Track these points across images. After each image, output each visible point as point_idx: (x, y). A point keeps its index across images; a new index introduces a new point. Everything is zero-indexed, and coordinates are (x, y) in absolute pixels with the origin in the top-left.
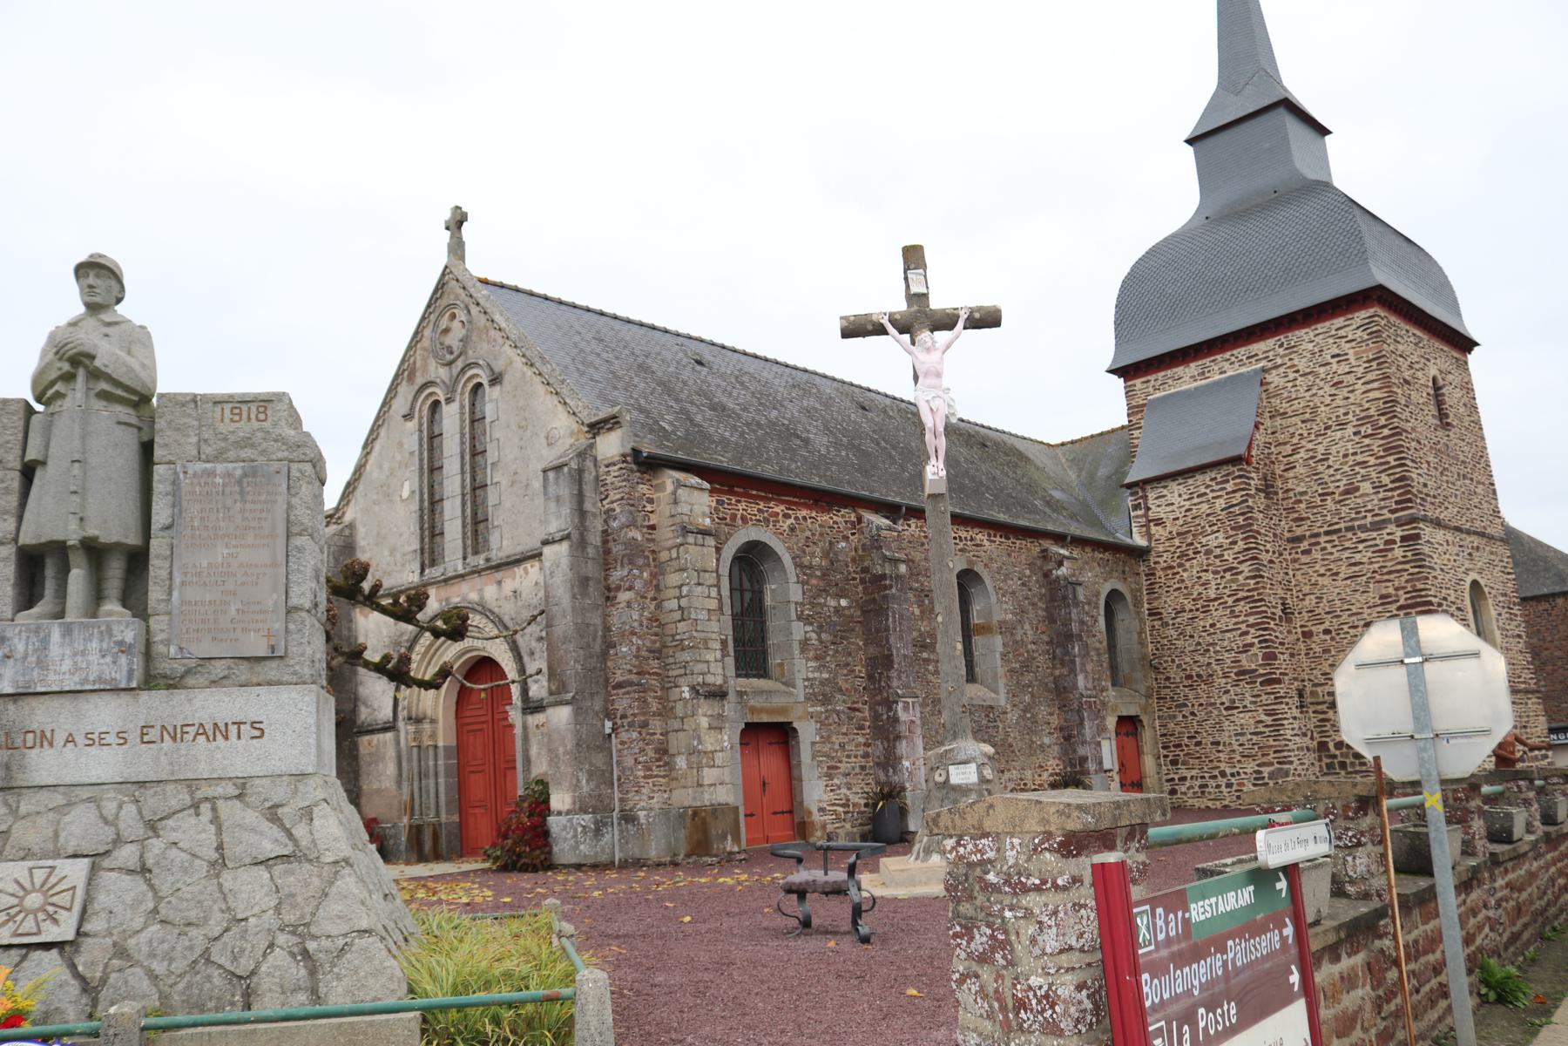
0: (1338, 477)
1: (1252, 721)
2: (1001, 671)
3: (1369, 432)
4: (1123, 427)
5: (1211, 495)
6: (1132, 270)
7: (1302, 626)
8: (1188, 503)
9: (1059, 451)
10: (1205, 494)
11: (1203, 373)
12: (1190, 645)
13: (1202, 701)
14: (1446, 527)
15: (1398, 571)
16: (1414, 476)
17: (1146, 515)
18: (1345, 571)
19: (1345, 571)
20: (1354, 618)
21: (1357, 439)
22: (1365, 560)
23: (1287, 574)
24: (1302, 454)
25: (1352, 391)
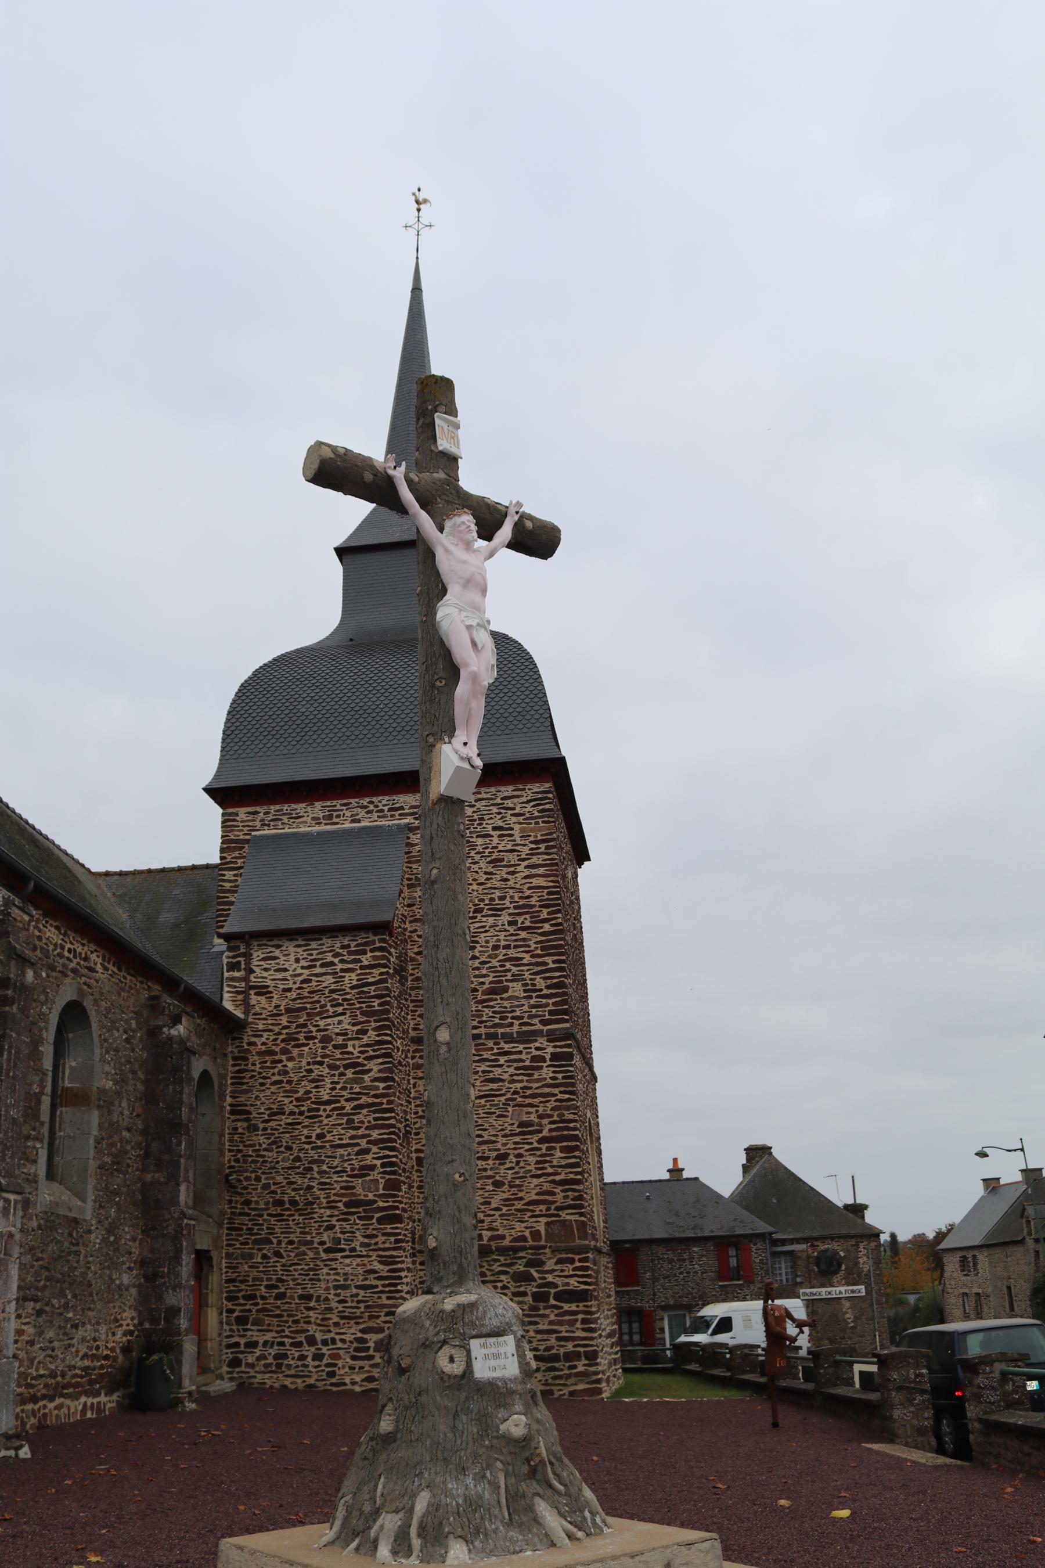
0: (484, 972)
1: (360, 1270)
2: (93, 1165)
3: (528, 924)
4: (207, 866)
5: (340, 966)
7: (417, 1151)
8: (306, 972)
9: (101, 881)
10: (332, 964)
11: (330, 817)
12: (285, 1160)
13: (292, 1237)
17: (246, 979)
20: (485, 1147)
21: (511, 929)
22: (506, 1076)
25: (513, 873)
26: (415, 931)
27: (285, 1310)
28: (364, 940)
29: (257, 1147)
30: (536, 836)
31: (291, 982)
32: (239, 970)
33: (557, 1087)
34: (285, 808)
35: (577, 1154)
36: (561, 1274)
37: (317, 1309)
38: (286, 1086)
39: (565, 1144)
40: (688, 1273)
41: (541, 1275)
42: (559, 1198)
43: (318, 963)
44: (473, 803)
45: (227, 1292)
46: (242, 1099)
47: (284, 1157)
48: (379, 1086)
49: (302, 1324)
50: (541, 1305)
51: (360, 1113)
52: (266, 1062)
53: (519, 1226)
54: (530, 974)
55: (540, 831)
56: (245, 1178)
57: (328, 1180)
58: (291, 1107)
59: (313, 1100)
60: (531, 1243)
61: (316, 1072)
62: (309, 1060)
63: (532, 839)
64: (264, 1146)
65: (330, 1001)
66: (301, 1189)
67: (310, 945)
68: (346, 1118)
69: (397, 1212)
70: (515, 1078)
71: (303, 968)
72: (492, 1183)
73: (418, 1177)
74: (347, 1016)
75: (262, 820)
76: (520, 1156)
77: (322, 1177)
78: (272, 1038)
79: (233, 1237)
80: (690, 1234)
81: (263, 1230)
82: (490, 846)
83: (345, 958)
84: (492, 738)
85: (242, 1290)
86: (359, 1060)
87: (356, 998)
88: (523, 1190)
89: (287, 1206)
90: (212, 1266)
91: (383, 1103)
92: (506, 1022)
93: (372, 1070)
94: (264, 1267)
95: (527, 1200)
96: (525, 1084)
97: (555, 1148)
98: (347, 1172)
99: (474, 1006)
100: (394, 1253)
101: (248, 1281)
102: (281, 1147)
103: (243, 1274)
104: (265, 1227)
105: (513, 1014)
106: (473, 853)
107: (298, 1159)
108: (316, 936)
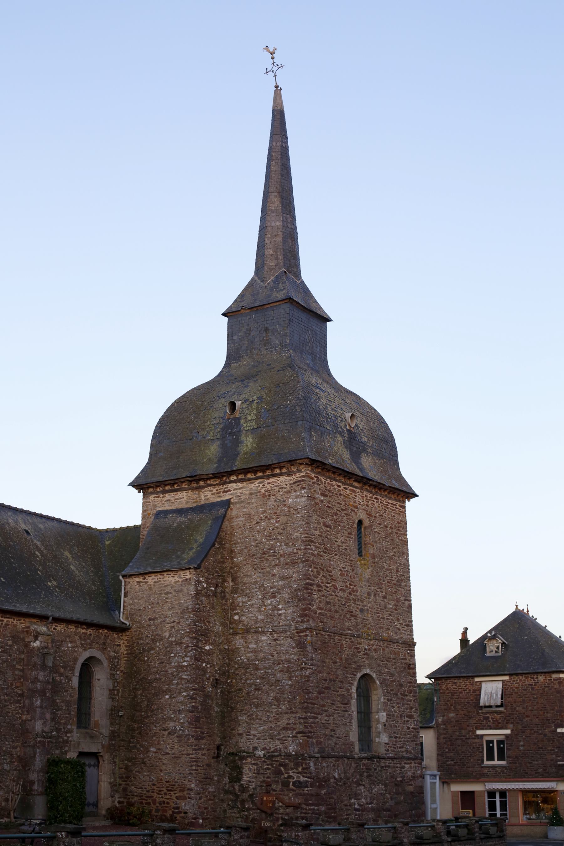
49: (150, 793)
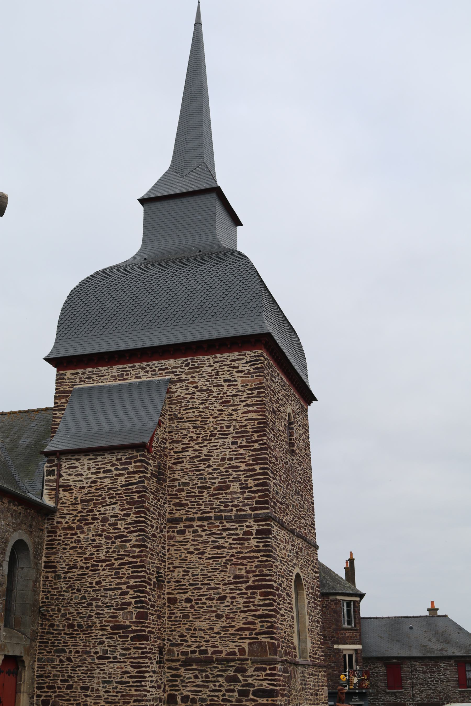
0: (215, 475)
1: (119, 671)
3: (244, 443)
4: (47, 409)
5: (115, 472)
6: (80, 284)
7: (168, 593)
8: (94, 476)
10: (110, 471)
11: (122, 375)
13: (79, 648)
14: (286, 529)
15: (250, 558)
16: (272, 484)
17: (57, 481)
18: (209, 552)
19: (209, 552)
20: (211, 591)
21: (234, 447)
22: (226, 545)
23: (163, 548)
24: (190, 452)
25: (236, 410)
26: (173, 449)
27: (72, 697)
28: (131, 455)
29: (60, 590)
30: (251, 385)
31: (85, 483)
32: (54, 475)
33: (259, 552)
34: (95, 370)
35: (271, 597)
36: (257, 678)
37: (91, 696)
38: (79, 550)
39: (263, 590)
40: (437, 681)
41: (244, 679)
42: (258, 627)
43: (102, 470)
44: (212, 364)
45: (37, 684)
46: (52, 558)
47: (76, 596)
48: (135, 551)
50: (244, 699)
51: (123, 568)
52: (67, 534)
53: (232, 645)
54: (245, 477)
55: (254, 382)
56: (51, 610)
57: (101, 612)
58: (82, 564)
59: (95, 559)
60: (239, 656)
61: (97, 540)
62: (94, 533)
63: (249, 387)
64: (64, 589)
65: (108, 495)
66: (85, 617)
67: (97, 459)
68: (114, 571)
69: (144, 633)
70: (233, 546)
71: (92, 473)
72: (215, 616)
73: (169, 610)
74: (118, 505)
75: (80, 378)
76: (234, 598)
77: (98, 610)
78: (71, 519)
79: (43, 648)
80: (438, 654)
81: (60, 643)
82: (222, 392)
83: (118, 467)
84: (225, 321)
85: (46, 683)
86: (124, 534)
87: (124, 493)
88: (235, 621)
89: (76, 628)
90: (25, 667)
91: (137, 562)
92: (228, 509)
93: (132, 540)
94: (60, 668)
95: (237, 628)
96: (239, 550)
97: (256, 593)
98: (114, 606)
99: (208, 498)
100: (141, 661)
101: (50, 677)
102: (74, 589)
103: (47, 672)
104: (62, 642)
105: (233, 503)
106: (211, 397)
107: (84, 597)
108: (101, 453)
